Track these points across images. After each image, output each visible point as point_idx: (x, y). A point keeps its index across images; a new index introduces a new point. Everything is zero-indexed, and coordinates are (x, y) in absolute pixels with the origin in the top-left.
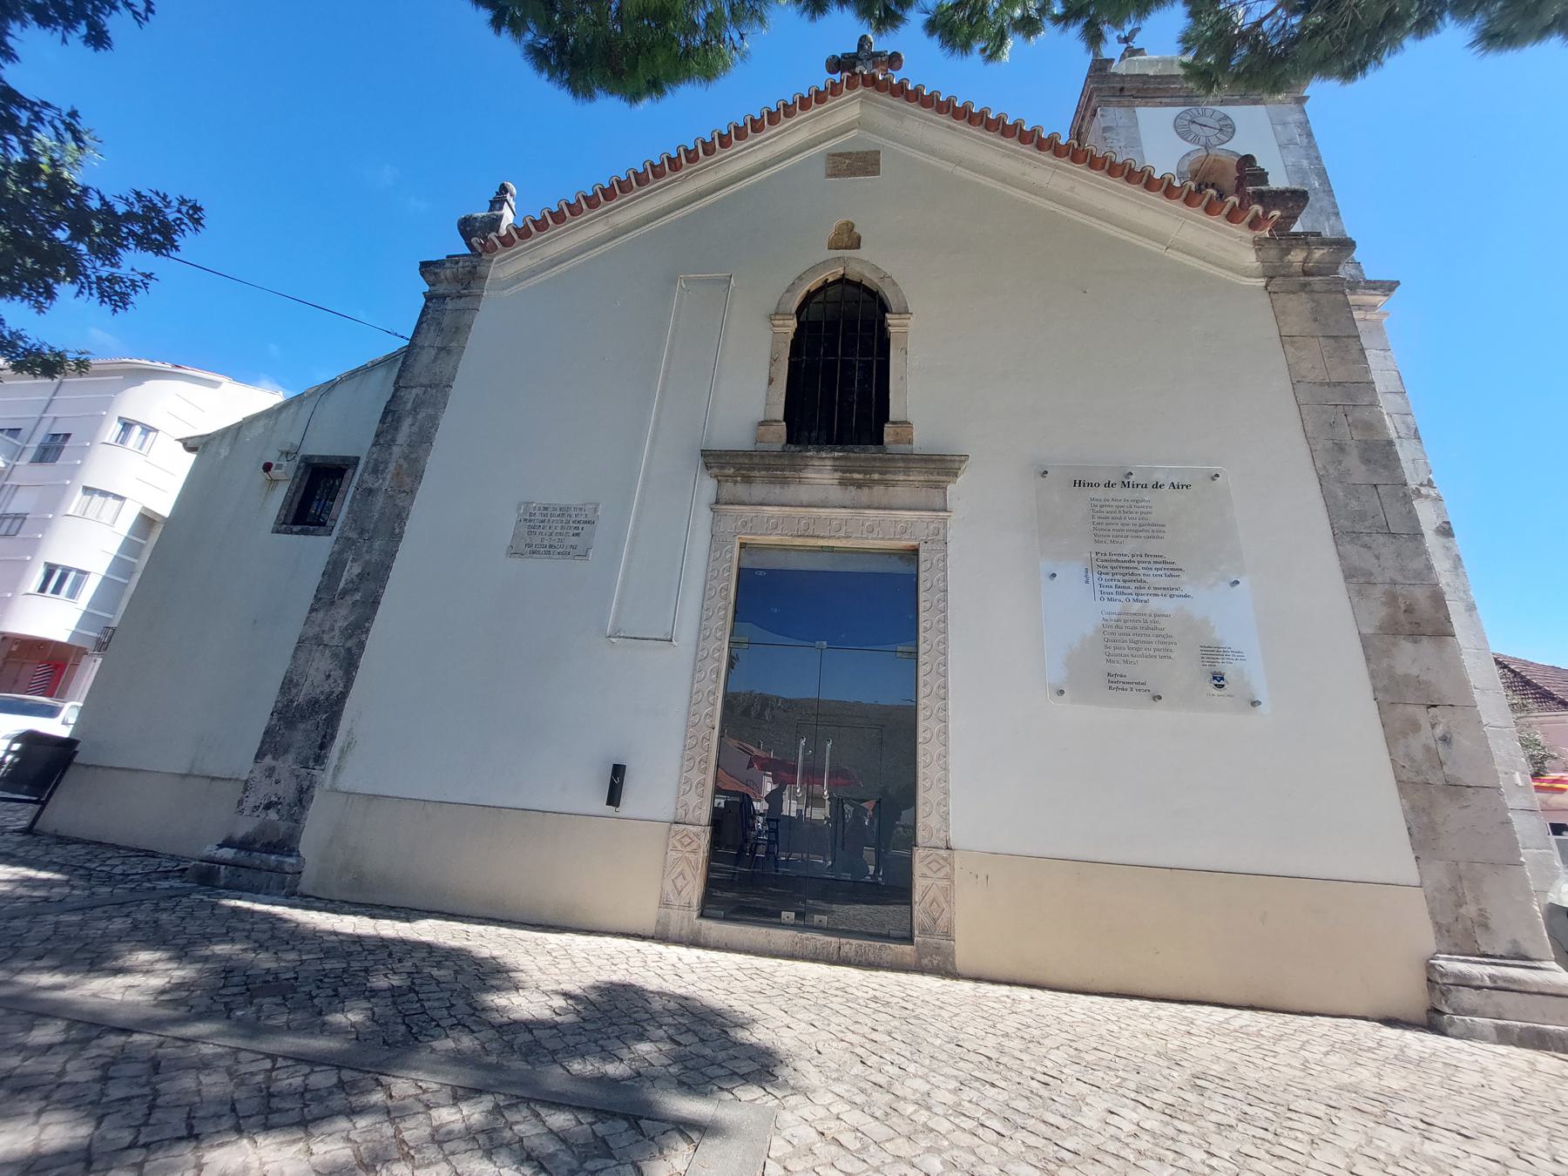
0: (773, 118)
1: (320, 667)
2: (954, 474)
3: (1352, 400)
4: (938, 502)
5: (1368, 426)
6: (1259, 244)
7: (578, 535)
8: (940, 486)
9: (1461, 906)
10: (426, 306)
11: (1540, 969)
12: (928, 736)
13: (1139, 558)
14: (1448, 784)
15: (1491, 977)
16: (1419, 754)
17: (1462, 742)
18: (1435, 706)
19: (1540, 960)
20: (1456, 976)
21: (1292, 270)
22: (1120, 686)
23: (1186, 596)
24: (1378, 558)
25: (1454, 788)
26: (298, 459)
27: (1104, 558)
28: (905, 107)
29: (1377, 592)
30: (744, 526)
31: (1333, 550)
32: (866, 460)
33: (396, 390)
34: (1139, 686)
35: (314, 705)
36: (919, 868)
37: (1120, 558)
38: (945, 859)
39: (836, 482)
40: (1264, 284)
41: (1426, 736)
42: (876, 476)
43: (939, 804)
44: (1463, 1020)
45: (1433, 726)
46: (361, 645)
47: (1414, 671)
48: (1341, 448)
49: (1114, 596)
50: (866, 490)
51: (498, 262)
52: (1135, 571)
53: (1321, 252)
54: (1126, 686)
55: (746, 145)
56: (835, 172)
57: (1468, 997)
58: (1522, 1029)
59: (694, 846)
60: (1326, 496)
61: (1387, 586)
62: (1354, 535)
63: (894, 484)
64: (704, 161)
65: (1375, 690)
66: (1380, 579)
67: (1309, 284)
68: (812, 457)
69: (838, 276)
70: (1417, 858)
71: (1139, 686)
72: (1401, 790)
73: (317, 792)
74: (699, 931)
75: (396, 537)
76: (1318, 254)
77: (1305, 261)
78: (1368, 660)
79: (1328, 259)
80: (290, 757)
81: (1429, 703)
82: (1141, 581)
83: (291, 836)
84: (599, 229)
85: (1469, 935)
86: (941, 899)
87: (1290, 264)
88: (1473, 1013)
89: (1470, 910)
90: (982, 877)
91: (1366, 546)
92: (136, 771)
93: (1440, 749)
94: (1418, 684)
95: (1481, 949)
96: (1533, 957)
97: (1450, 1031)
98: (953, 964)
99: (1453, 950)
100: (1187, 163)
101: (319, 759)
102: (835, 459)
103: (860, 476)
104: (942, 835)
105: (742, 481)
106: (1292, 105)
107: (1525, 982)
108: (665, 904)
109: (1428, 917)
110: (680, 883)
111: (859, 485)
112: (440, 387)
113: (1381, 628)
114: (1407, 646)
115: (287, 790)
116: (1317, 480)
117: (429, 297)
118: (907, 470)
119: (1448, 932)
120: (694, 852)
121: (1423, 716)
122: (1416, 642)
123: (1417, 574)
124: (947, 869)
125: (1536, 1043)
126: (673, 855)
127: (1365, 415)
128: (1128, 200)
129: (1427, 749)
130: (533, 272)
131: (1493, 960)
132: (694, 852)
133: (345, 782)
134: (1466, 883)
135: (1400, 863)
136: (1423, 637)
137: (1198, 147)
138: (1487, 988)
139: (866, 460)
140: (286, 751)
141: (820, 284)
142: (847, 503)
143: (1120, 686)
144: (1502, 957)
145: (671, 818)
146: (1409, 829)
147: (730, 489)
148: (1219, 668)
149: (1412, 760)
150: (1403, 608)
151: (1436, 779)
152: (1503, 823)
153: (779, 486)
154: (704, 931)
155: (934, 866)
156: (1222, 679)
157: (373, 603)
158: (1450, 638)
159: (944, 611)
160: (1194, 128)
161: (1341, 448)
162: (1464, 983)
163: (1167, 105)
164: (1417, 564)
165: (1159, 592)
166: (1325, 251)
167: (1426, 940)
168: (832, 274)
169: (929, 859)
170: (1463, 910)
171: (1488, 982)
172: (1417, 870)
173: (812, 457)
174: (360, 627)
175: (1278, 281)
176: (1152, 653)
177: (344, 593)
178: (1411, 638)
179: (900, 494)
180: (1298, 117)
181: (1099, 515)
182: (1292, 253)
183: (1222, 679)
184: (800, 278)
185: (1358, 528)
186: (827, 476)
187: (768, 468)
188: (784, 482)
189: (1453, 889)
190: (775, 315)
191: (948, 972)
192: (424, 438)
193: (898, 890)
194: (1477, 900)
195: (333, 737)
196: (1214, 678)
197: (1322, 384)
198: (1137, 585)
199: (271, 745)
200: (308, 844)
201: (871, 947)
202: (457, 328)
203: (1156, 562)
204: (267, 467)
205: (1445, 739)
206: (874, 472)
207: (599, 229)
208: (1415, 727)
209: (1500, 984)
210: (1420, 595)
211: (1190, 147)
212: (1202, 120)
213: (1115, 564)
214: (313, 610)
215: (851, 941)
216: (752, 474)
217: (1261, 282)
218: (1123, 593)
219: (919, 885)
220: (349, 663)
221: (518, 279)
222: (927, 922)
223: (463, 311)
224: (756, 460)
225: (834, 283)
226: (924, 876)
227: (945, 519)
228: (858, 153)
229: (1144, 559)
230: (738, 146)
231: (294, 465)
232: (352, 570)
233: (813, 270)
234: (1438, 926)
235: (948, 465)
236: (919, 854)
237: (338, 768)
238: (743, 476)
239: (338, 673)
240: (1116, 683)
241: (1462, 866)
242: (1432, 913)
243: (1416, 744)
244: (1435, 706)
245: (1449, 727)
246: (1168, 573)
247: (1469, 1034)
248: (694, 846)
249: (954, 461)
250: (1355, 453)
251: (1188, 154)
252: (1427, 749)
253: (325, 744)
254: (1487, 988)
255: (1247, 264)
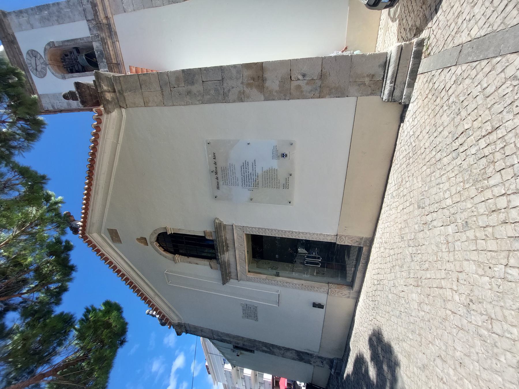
0: (106, 259)
1: (288, 354)
2: (220, 224)
3: (167, 83)
4: (231, 227)
5: (177, 79)
6: (108, 112)
7: (250, 308)
8: (225, 226)
9: (365, 84)
10: (190, 333)
11: (390, 60)
12: (304, 237)
13: (243, 173)
14: (321, 78)
15: (391, 83)
16: (309, 88)
17: (305, 69)
18: (291, 77)
19: (387, 58)
20: (389, 96)
21: (114, 96)
22: (287, 186)
23: (255, 161)
24: (233, 88)
25: (322, 76)
26: (234, 349)
27: (244, 184)
28: (89, 223)
29: (247, 91)
30: (244, 274)
31: (231, 104)
32: (220, 247)
33: (215, 340)
34: (287, 180)
35: (298, 355)
36: (342, 243)
37: (243, 179)
38: (340, 237)
39: (227, 252)
40: (124, 109)
41: (302, 83)
42: (224, 244)
43: (324, 236)
44: (404, 99)
45: (299, 79)
46: (283, 347)
47: (277, 83)
48: (189, 93)
49: (257, 183)
50: (229, 245)
51: (173, 321)
52: (247, 175)
53: (104, 86)
54: (287, 184)
55: (118, 265)
56: (119, 241)
57: (397, 93)
58: (410, 78)
59: (334, 291)
60: (209, 102)
61: (245, 86)
62: (225, 95)
63: (226, 238)
64: (127, 276)
65: (285, 99)
66: (242, 88)
67: (119, 91)
68: (221, 260)
69: (157, 243)
70: (347, 96)
71: (287, 180)
72: (322, 98)
73: (319, 355)
74: (356, 291)
75: (255, 341)
76: (105, 88)
77: (109, 92)
78: (274, 100)
79: (106, 83)
80: (311, 359)
81: (290, 79)
82: (251, 174)
83: (329, 359)
84: (157, 299)
85: (376, 83)
86: (351, 239)
87: (112, 98)
88: (402, 92)
89: (367, 80)
90: (345, 228)
91: (229, 91)
92: (313, 373)
93: (307, 79)
94: (282, 82)
95: (381, 79)
96: (385, 61)
97: (407, 104)
98: (369, 238)
99: (380, 90)
100: (57, 74)
101: (311, 355)
102: (221, 255)
103: (225, 248)
104: (333, 236)
105: (230, 273)
106: (9, 18)
107: (394, 71)
108: (349, 297)
109: (368, 97)
110: (343, 294)
111: (227, 247)
112: (212, 332)
113: (261, 92)
114: (268, 84)
115: (319, 360)
116: (204, 104)
117: (187, 333)
118: (221, 236)
119: (374, 91)
120: (336, 291)
121: (294, 84)
122: (266, 80)
123: (238, 72)
124: (343, 237)
125: (415, 74)
126: (336, 295)
127: (173, 79)
128: (103, 157)
129: (307, 84)
130: (174, 312)
131: (385, 77)
132: (336, 291)
133: (317, 350)
134: (357, 80)
135: (348, 103)
136: (264, 76)
137: (47, 68)
138: (394, 86)
139: (220, 247)
140: (309, 360)
141: (161, 248)
142: (234, 250)
143: (287, 186)
144: (384, 72)
145: (326, 295)
146: (336, 97)
147: (233, 275)
148: (279, 154)
149: (311, 90)
150: (253, 81)
151: (319, 83)
152: (336, 60)
153: (231, 266)
154: (356, 290)
155: (342, 240)
156: (283, 154)
157: (273, 346)
158: (263, 65)
159: (265, 229)
160: (39, 68)
161: (189, 93)
162: (392, 93)
163: (32, 80)
164: (234, 72)
165: (254, 169)
166: (103, 85)
167: (375, 99)
168: (156, 245)
169: (340, 241)
170: (367, 83)
171: (392, 85)
172: (352, 97)
173: (221, 260)
174: (279, 348)
175: (121, 105)
176: (276, 175)
177: (270, 350)
178: (264, 81)
179: (229, 236)
180: (13, 16)
181: (229, 183)
182: (108, 99)
183: (283, 154)
184: (161, 254)
185: (222, 92)
186: (226, 255)
187: (226, 269)
188: (229, 265)
189: (359, 85)
190: (174, 260)
191: (371, 241)
192: (228, 335)
193: (347, 248)
194: (364, 77)
195: (306, 352)
196: (283, 157)
197: (163, 94)
198: (252, 176)
199: (309, 362)
200: (331, 357)
201: (362, 261)
202: (195, 328)
203: (244, 169)
204: (238, 355)
205: (304, 75)
206: (223, 245)
207: (157, 299)
208: (299, 87)
209: (393, 80)
210: (246, 73)
211: (49, 73)
212: (34, 65)
213: (246, 182)
214: (275, 355)
215: (361, 260)
216: (228, 272)
217: (123, 110)
218: (255, 180)
219: (346, 244)
220: (288, 349)
221: (177, 316)
222: (357, 243)
223: (190, 327)
224: (224, 273)
225: (159, 244)
226: (344, 242)
227: (236, 226)
228: (110, 235)
229: (243, 172)
230: (119, 267)
231: (236, 350)
232: (264, 348)
233: (157, 251)
234: (372, 94)
235: (218, 226)
236: (338, 243)
237: (313, 352)
238: (229, 274)
239: (291, 352)
240: (286, 186)
241: (351, 80)
242: (367, 95)
243: (306, 88)
244: (291, 77)
245: (299, 73)
246: (247, 165)
247: (409, 97)
248: (334, 291)
249: (217, 225)
250: (190, 87)
251: (53, 73)
252: (307, 84)
253: (308, 354)
254: (394, 86)
255: (117, 114)
